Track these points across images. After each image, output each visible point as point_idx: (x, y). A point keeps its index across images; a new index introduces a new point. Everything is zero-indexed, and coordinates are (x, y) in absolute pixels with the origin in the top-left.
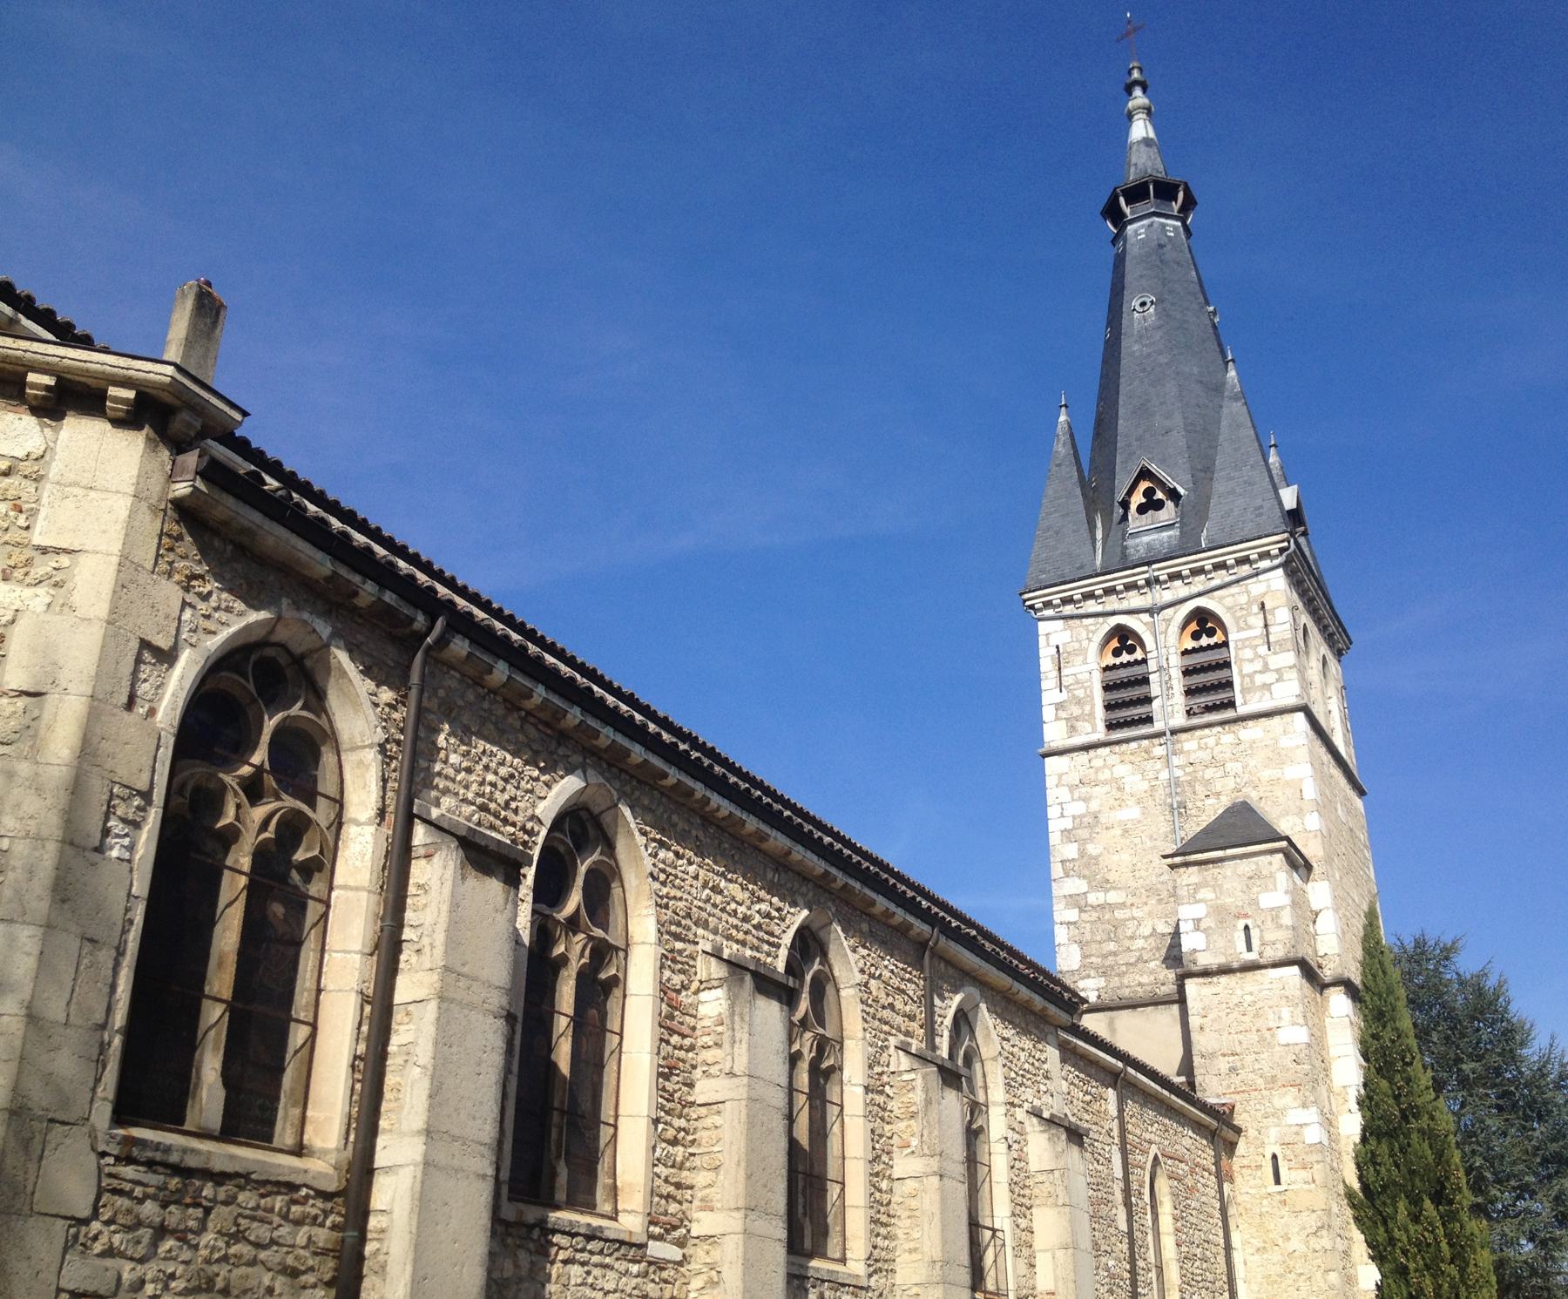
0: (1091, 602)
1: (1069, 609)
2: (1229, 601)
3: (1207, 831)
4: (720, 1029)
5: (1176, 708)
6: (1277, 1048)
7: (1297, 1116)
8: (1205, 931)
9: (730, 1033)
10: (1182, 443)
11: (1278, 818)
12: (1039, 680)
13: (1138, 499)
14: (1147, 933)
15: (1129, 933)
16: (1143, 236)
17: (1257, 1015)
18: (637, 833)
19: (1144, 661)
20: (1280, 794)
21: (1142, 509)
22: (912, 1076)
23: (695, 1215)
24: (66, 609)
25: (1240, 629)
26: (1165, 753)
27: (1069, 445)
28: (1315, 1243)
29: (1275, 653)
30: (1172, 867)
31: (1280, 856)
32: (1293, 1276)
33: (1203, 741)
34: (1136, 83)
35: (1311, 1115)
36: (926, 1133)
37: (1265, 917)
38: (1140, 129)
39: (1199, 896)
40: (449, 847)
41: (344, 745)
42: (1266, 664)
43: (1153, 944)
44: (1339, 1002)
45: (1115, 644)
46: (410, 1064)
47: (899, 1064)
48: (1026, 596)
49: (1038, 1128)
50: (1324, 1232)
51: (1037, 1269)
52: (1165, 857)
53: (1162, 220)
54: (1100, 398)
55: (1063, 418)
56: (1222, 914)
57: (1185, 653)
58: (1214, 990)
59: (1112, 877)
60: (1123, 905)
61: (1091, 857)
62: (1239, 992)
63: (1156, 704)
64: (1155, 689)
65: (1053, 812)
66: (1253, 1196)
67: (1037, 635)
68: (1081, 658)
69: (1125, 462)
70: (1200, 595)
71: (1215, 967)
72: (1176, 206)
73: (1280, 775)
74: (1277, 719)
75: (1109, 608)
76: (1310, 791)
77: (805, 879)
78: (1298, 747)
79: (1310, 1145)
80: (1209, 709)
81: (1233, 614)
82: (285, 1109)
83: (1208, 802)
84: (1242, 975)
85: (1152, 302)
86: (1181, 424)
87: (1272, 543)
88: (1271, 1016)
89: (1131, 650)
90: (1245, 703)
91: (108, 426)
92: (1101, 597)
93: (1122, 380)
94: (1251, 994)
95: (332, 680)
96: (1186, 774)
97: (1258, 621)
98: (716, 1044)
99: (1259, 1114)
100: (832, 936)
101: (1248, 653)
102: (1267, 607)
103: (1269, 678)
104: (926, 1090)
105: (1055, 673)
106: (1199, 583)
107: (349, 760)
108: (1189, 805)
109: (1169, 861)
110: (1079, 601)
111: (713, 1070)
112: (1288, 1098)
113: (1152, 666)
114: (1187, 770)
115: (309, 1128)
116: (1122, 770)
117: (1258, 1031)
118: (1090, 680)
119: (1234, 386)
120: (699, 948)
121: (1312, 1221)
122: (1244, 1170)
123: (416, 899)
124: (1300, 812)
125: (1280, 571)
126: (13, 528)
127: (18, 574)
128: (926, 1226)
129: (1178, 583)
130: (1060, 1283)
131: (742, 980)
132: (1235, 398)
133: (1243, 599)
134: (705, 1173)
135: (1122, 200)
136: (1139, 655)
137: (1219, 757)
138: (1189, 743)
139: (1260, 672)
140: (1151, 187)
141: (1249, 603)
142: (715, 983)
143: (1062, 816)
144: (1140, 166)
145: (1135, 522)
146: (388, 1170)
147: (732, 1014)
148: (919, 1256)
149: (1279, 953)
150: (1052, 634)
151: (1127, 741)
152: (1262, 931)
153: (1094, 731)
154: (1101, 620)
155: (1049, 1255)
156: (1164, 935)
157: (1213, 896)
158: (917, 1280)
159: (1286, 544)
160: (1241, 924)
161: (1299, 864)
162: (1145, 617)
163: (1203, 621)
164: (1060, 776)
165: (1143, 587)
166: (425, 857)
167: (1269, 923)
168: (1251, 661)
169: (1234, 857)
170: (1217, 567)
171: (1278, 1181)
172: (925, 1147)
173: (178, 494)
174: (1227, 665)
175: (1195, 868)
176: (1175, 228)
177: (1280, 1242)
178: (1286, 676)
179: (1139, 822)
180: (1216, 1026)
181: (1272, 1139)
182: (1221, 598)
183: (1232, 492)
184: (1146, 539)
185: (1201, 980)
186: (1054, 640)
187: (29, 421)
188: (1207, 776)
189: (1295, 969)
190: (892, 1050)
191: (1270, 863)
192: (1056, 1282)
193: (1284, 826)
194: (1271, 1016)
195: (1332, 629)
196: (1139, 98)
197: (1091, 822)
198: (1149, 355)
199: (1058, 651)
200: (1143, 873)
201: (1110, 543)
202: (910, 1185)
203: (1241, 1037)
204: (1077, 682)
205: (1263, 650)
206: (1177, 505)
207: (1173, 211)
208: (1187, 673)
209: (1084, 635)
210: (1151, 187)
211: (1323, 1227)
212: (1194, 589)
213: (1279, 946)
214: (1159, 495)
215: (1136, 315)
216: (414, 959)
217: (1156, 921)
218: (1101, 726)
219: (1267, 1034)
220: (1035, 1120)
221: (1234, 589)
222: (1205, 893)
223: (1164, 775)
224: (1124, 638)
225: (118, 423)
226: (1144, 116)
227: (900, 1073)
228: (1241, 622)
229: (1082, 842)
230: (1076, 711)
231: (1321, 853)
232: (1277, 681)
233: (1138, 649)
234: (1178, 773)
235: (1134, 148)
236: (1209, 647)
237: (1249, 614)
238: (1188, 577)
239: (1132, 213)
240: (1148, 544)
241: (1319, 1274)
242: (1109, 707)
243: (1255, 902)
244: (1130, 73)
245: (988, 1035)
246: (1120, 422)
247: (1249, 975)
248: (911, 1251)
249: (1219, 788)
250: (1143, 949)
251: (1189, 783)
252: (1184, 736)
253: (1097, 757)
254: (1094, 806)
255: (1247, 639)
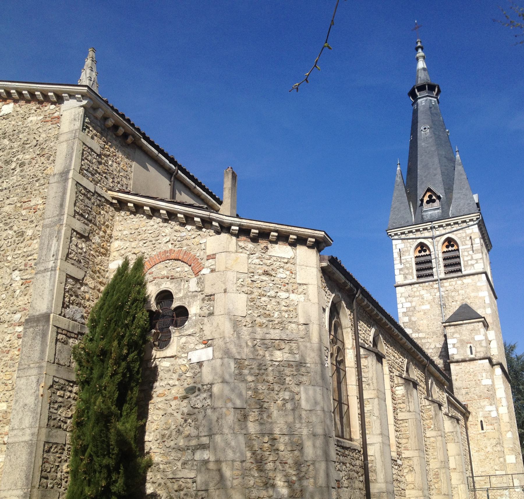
0: (411, 234)
1: (403, 236)
2: (459, 235)
3: (455, 314)
4: (404, 398)
5: (441, 271)
6: (482, 386)
7: (488, 408)
8: (456, 348)
9: (407, 399)
10: (441, 179)
12: (393, 261)
13: (426, 199)
14: (433, 347)
15: (427, 347)
16: (424, 104)
17: (474, 376)
18: (383, 344)
19: (430, 255)
20: (477, 301)
21: (428, 202)
22: (430, 407)
23: (403, 452)
24: (308, 301)
25: (463, 245)
26: (438, 287)
27: (401, 178)
28: (495, 449)
29: (475, 254)
31: (482, 323)
32: (488, 459)
33: (451, 283)
34: (419, 47)
35: (493, 408)
36: (436, 424)
38: (421, 64)
39: (454, 336)
40: (372, 355)
41: (343, 328)
42: (472, 257)
43: (435, 351)
44: (498, 370)
45: (419, 248)
46: (372, 415)
47: (425, 403)
48: (388, 231)
49: (447, 419)
50: (498, 445)
51: (450, 461)
53: (431, 98)
54: (409, 161)
55: (398, 168)
56: (462, 342)
57: (444, 252)
58: (460, 367)
59: (420, 328)
60: (424, 338)
61: (413, 321)
62: (468, 368)
63: (434, 270)
64: (434, 265)
65: (399, 306)
66: (475, 434)
67: (392, 245)
68: (408, 253)
69: (421, 185)
70: (449, 233)
71: (460, 360)
72: (435, 93)
73: (477, 295)
74: (476, 276)
75: (417, 236)
76: (487, 301)
77: (405, 350)
78: (483, 286)
79: (493, 418)
80: (452, 272)
81: (461, 240)
82: (345, 428)
83: (453, 303)
84: (470, 362)
85: (428, 128)
86: (440, 172)
87: (474, 216)
88: (479, 376)
89: (425, 251)
90: (465, 270)
91: (307, 248)
92: (414, 232)
93: (418, 155)
94: (472, 368)
95: (341, 310)
96: (445, 294)
97: (469, 243)
98: (403, 402)
99: (476, 408)
100: (410, 366)
101: (466, 254)
102: (472, 238)
103: (473, 262)
104: (435, 411)
105: (399, 258)
106: (449, 229)
107: (344, 331)
108: (447, 304)
109: (444, 324)
110: (407, 234)
111: (403, 410)
112: (485, 402)
113: (433, 256)
114: (446, 293)
115: (352, 434)
116: (423, 292)
117: (475, 380)
118: (411, 261)
119: (459, 160)
120: (395, 374)
121: (494, 442)
122: (472, 426)
123: (364, 370)
124: (484, 308)
125: (476, 226)
126: (291, 278)
127: (295, 291)
128: (438, 451)
129: (441, 228)
130: (457, 466)
131: (409, 384)
132: (460, 165)
133: (464, 235)
134: (404, 440)
135: (416, 90)
136: (428, 252)
137: (457, 288)
138: (446, 283)
139: (470, 260)
140: (427, 86)
141: (466, 236)
142: (401, 385)
143: (403, 307)
144: (422, 78)
145: (426, 207)
146: (371, 444)
147: (408, 394)
148: (437, 460)
149: (482, 355)
150: (397, 245)
151: (425, 282)
152: (476, 348)
153: (413, 278)
154: (415, 240)
155: (453, 457)
156: (439, 348)
157: (459, 336)
158: (437, 467)
159: (479, 217)
160: (469, 345)
161: (486, 326)
162: (430, 240)
163: (450, 242)
164: (402, 294)
165: (429, 230)
166: (365, 358)
167: (478, 346)
168: (467, 256)
169: (466, 323)
170: (455, 223)
171: (482, 429)
172: (436, 428)
173: (322, 265)
174: (458, 257)
175: (453, 327)
176: (435, 101)
177: (484, 448)
178: (479, 262)
179: (429, 310)
180: (461, 379)
181: (481, 415)
182: (456, 235)
183: (460, 198)
184: (430, 213)
185: (456, 364)
186: (399, 246)
187: (289, 248)
188: (453, 295)
189: (487, 361)
190: (423, 399)
191: (478, 326)
192: (456, 465)
193: (480, 312)
194: (479, 376)
195: (488, 243)
196: (420, 53)
197: (412, 310)
198: (428, 147)
199: (400, 251)
200: (431, 327)
201: (417, 214)
202: (432, 439)
203: (469, 382)
204: (407, 262)
205: (471, 252)
206: (440, 201)
207: (433, 95)
208: (444, 259)
209: (409, 245)
210: (427, 86)
211: (498, 444)
212: (447, 231)
213: (482, 353)
214: (434, 197)
215: (423, 132)
216: (367, 386)
217: (436, 343)
218: (415, 277)
219: (478, 382)
220: (446, 417)
221: (461, 231)
222: (456, 335)
223: (438, 294)
224: (422, 247)
225: (309, 247)
226: (422, 59)
227: (426, 406)
228: (463, 242)
229: (410, 317)
230: (407, 272)
231: (491, 321)
232: (476, 263)
233: (427, 251)
234: (443, 294)
235: (419, 71)
236: (452, 251)
237: (466, 240)
238: (445, 227)
239: (420, 95)
240: (430, 214)
241: (497, 459)
242: (418, 270)
243: (473, 338)
244: (417, 43)
245: (435, 391)
246: (418, 170)
247: (472, 362)
248: (434, 459)
249: (457, 299)
250: (432, 352)
251: (446, 297)
252: (444, 281)
253: (414, 287)
254: (414, 304)
255: (465, 249)
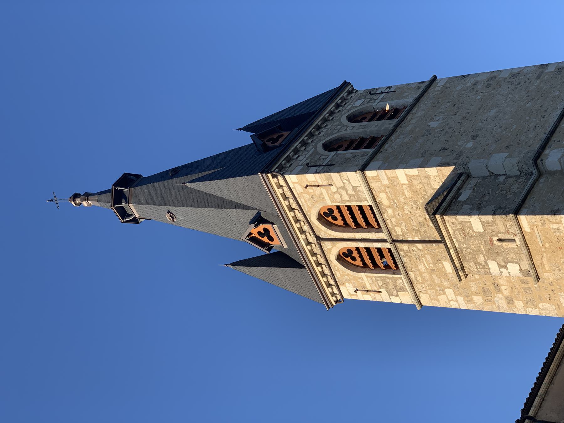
11: (434, 189)
30: (466, 276)
37: (489, 229)
39: (483, 263)
52: (460, 280)
90: (367, 200)
140: (117, 206)
150: (348, 292)
152: (499, 233)
205: (333, 189)
210: (117, 206)
222: (481, 259)
